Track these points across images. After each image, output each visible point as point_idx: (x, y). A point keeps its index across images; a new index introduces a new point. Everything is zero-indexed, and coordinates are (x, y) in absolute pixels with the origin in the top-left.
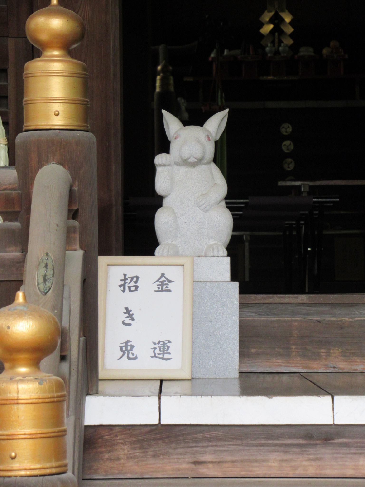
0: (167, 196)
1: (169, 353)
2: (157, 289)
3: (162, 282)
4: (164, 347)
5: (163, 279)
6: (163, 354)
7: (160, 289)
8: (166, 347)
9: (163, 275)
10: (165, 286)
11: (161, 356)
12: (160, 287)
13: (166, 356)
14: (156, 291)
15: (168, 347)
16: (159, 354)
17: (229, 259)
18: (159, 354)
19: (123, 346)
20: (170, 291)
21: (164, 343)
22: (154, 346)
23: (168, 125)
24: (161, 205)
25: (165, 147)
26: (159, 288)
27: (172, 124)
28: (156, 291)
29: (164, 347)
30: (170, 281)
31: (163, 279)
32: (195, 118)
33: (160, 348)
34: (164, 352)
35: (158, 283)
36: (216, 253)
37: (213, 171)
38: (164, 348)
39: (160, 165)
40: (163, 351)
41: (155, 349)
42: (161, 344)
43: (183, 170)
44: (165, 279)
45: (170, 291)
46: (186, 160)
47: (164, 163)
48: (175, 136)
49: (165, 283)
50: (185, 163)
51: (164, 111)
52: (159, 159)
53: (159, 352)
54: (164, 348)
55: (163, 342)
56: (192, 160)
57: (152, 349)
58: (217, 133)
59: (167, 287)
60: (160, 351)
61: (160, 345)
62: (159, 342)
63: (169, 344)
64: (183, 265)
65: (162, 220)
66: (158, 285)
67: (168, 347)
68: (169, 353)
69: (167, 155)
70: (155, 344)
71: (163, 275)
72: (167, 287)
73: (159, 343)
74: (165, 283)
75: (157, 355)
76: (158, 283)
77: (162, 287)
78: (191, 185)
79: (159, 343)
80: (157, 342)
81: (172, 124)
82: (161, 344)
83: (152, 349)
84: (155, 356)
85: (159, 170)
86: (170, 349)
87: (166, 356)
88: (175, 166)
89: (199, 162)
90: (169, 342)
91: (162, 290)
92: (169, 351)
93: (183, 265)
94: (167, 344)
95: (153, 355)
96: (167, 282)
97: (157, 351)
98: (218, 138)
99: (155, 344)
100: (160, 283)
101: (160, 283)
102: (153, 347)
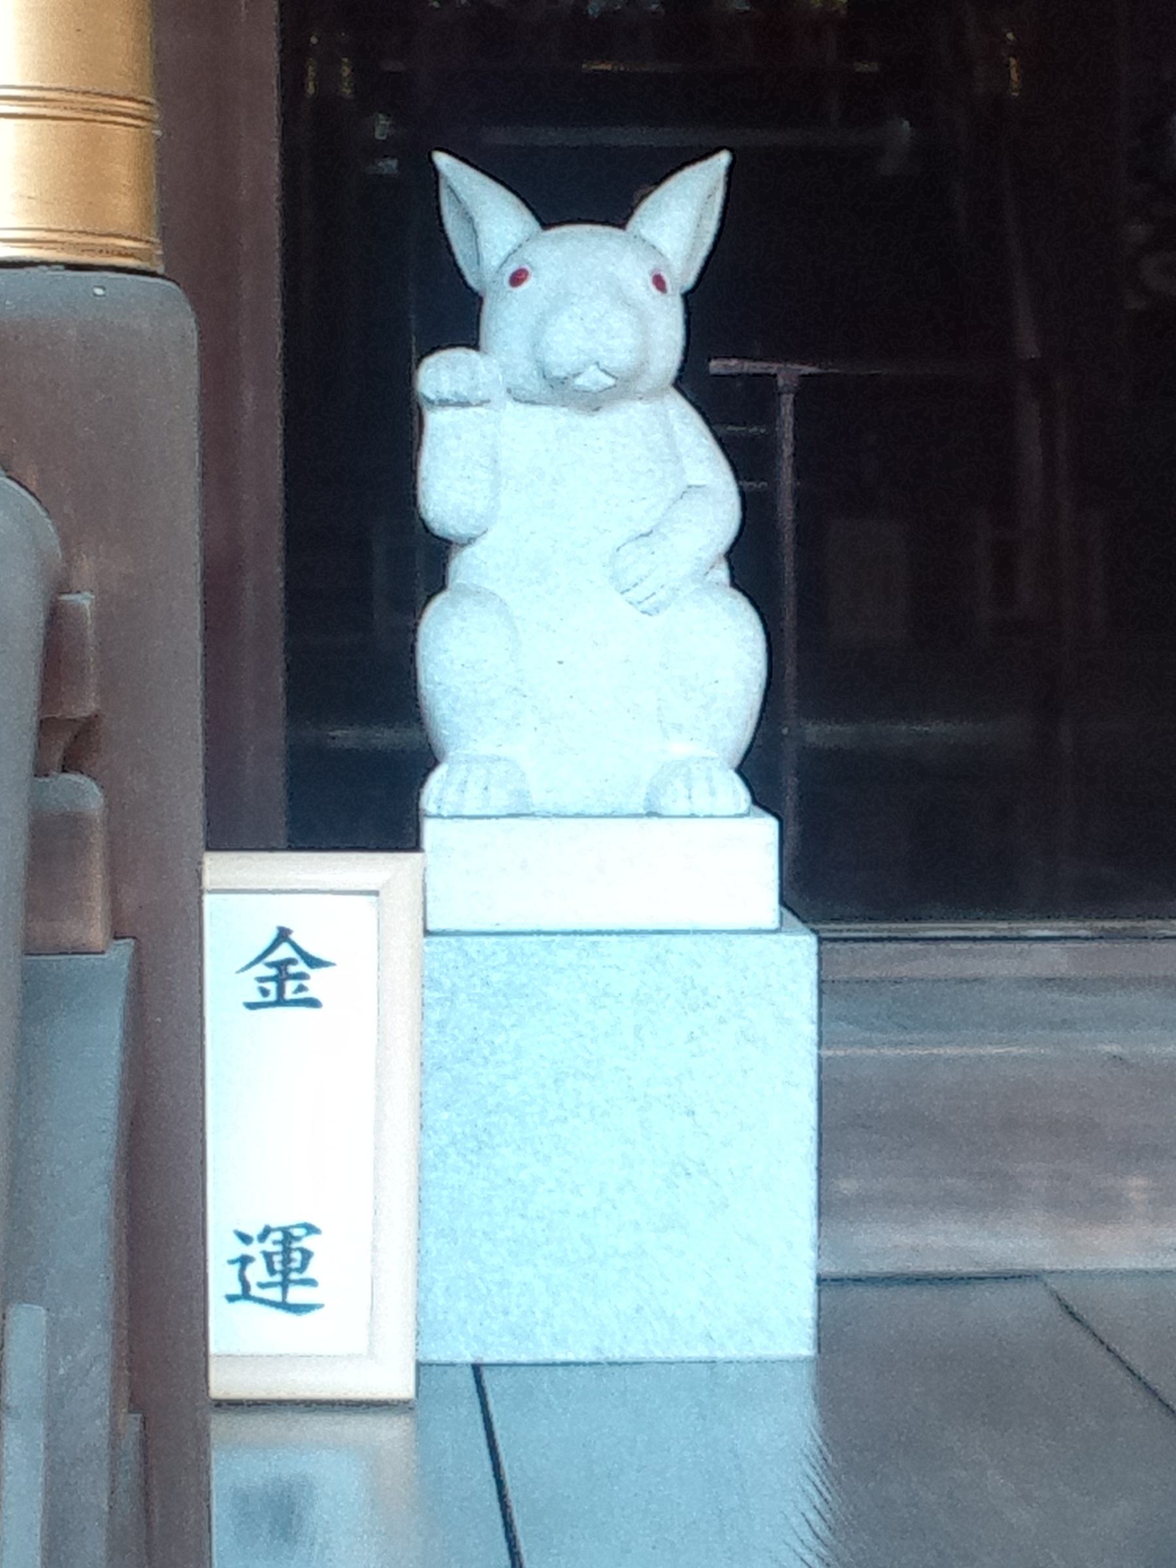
0: (471, 540)
1: (311, 1282)
2: (259, 998)
3: (281, 965)
4: (287, 1251)
5: (284, 952)
6: (285, 1285)
7: (272, 997)
8: (297, 1256)
9: (283, 935)
10: (291, 986)
11: (275, 1294)
12: (272, 986)
13: (296, 1295)
14: (252, 1006)
15: (307, 1255)
16: (262, 1286)
17: (767, 827)
18: (262, 1286)
19: (277, 1253)
20: (313, 1003)
21: (288, 1237)
22: (243, 1249)
23: (468, 219)
24: (437, 583)
25: (458, 318)
26: (265, 992)
27: (486, 219)
28: (252, 1006)
29: (287, 1251)
30: (314, 962)
31: (284, 952)
32: (586, 191)
33: (268, 1256)
34: (285, 1273)
35: (262, 970)
36: (701, 805)
37: (677, 426)
38: (287, 1261)
39: (444, 403)
40: (285, 1273)
41: (245, 1261)
42: (275, 1243)
43: (549, 419)
44: (292, 954)
45: (313, 1003)
46: (563, 381)
47: (463, 391)
48: (510, 269)
49: (292, 969)
50: (558, 389)
51: (442, 160)
52: (438, 374)
53: (266, 1278)
54: (287, 1261)
55: (286, 1231)
56: (592, 379)
57: (232, 1262)
58: (690, 258)
59: (301, 989)
60: (272, 1271)
61: (268, 1246)
62: (267, 1231)
63: (308, 1243)
64: (376, 893)
65: (454, 650)
66: (261, 980)
67: (307, 1255)
68: (311, 1282)
69: (473, 354)
70: (245, 1239)
71: (283, 935)
72: (301, 989)
73: (263, 1237)
74: (292, 969)
75: (255, 1291)
76: (262, 970)
77: (281, 990)
78: (584, 488)
79: (263, 1237)
80: (254, 1231)
81: (486, 219)
82: (275, 1243)
83: (232, 1262)
84: (246, 1294)
85: (436, 421)
86: (313, 1263)
87: (296, 1295)
88: (510, 405)
89: (623, 387)
90: (311, 1229)
91: (281, 1001)
92: (307, 1274)
93: (376, 893)
94: (298, 1239)
95: (237, 1289)
96: (301, 967)
97: (257, 1272)
98: (690, 280)
99: (245, 1239)
100: (273, 972)
101: (273, 972)
102: (236, 1255)
